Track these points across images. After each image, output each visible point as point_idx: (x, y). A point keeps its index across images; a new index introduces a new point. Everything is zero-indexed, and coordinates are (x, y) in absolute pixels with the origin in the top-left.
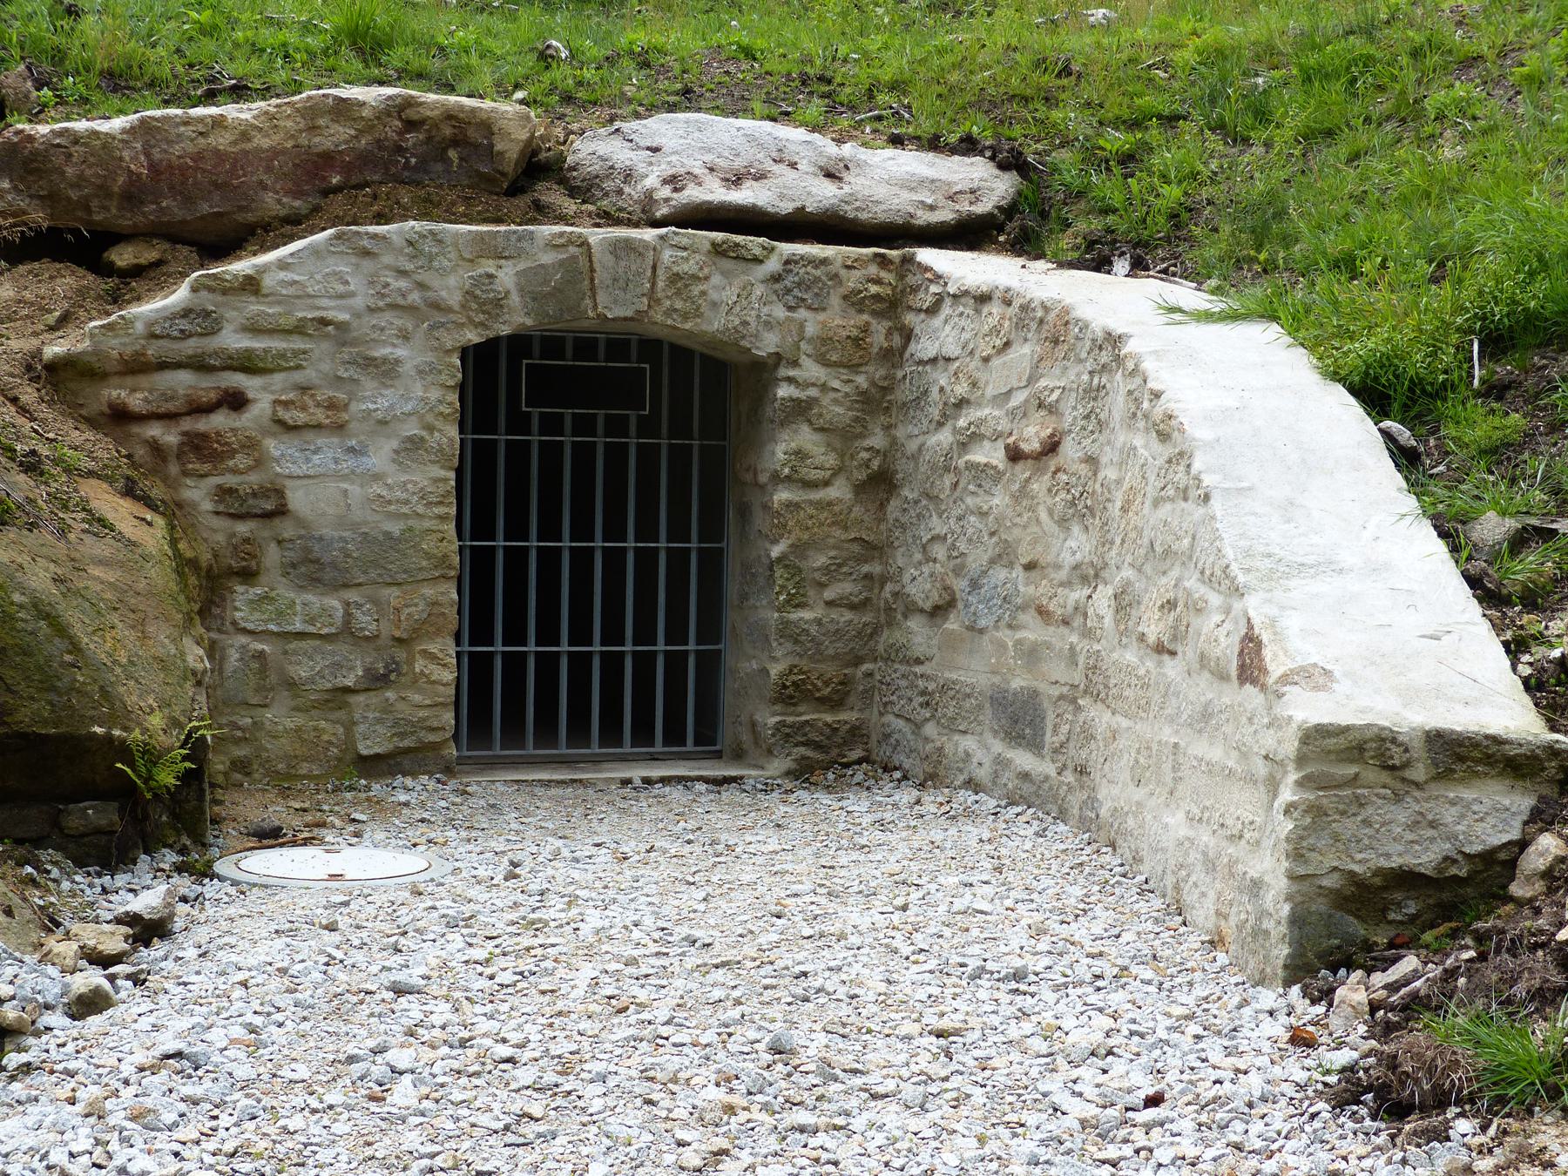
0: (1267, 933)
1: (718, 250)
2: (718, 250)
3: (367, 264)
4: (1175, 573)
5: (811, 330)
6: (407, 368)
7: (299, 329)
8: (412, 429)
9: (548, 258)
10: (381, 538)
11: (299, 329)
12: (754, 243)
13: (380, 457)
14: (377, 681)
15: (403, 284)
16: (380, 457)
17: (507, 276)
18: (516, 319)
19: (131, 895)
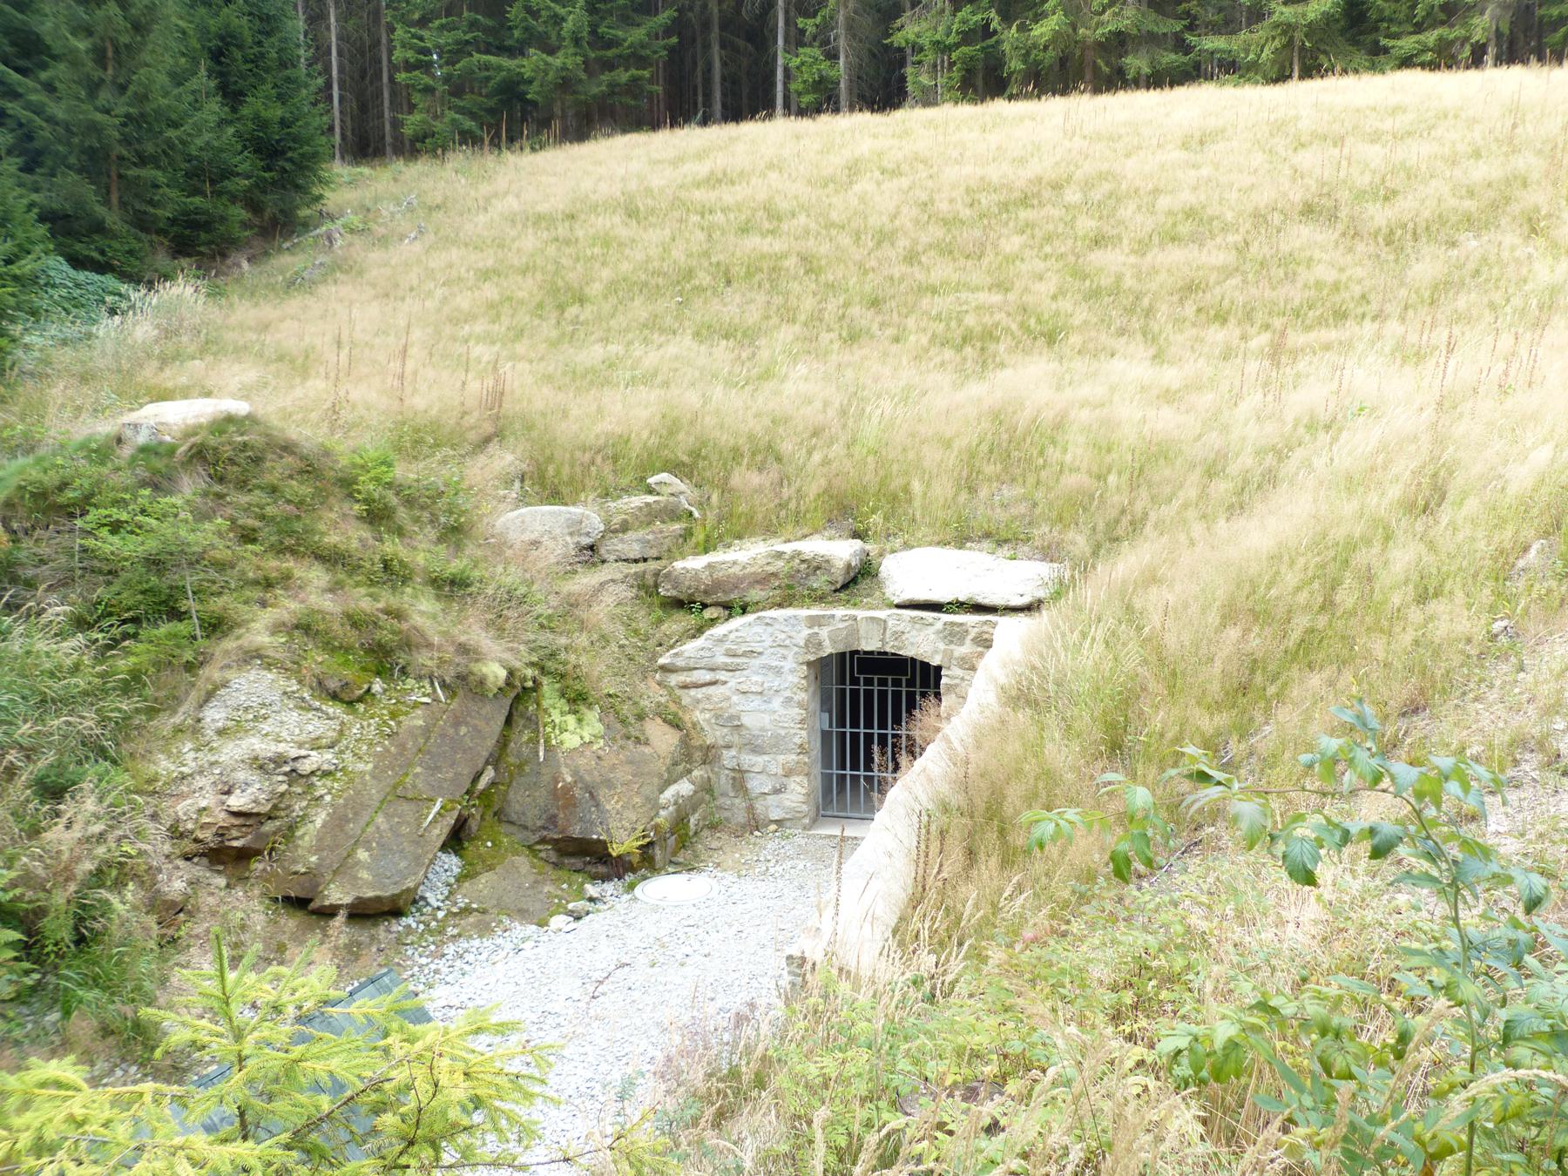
0: (909, 388)
1: (913, 620)
2: (913, 620)
3: (770, 629)
4: (799, 1067)
5: (956, 654)
6: (786, 669)
7: (744, 654)
8: (788, 693)
9: (841, 625)
10: (461, 693)
11: (744, 654)
12: (928, 615)
13: (777, 703)
14: (777, 791)
15: (783, 636)
16: (777, 703)
17: (824, 633)
18: (828, 649)
19: (1419, 721)
